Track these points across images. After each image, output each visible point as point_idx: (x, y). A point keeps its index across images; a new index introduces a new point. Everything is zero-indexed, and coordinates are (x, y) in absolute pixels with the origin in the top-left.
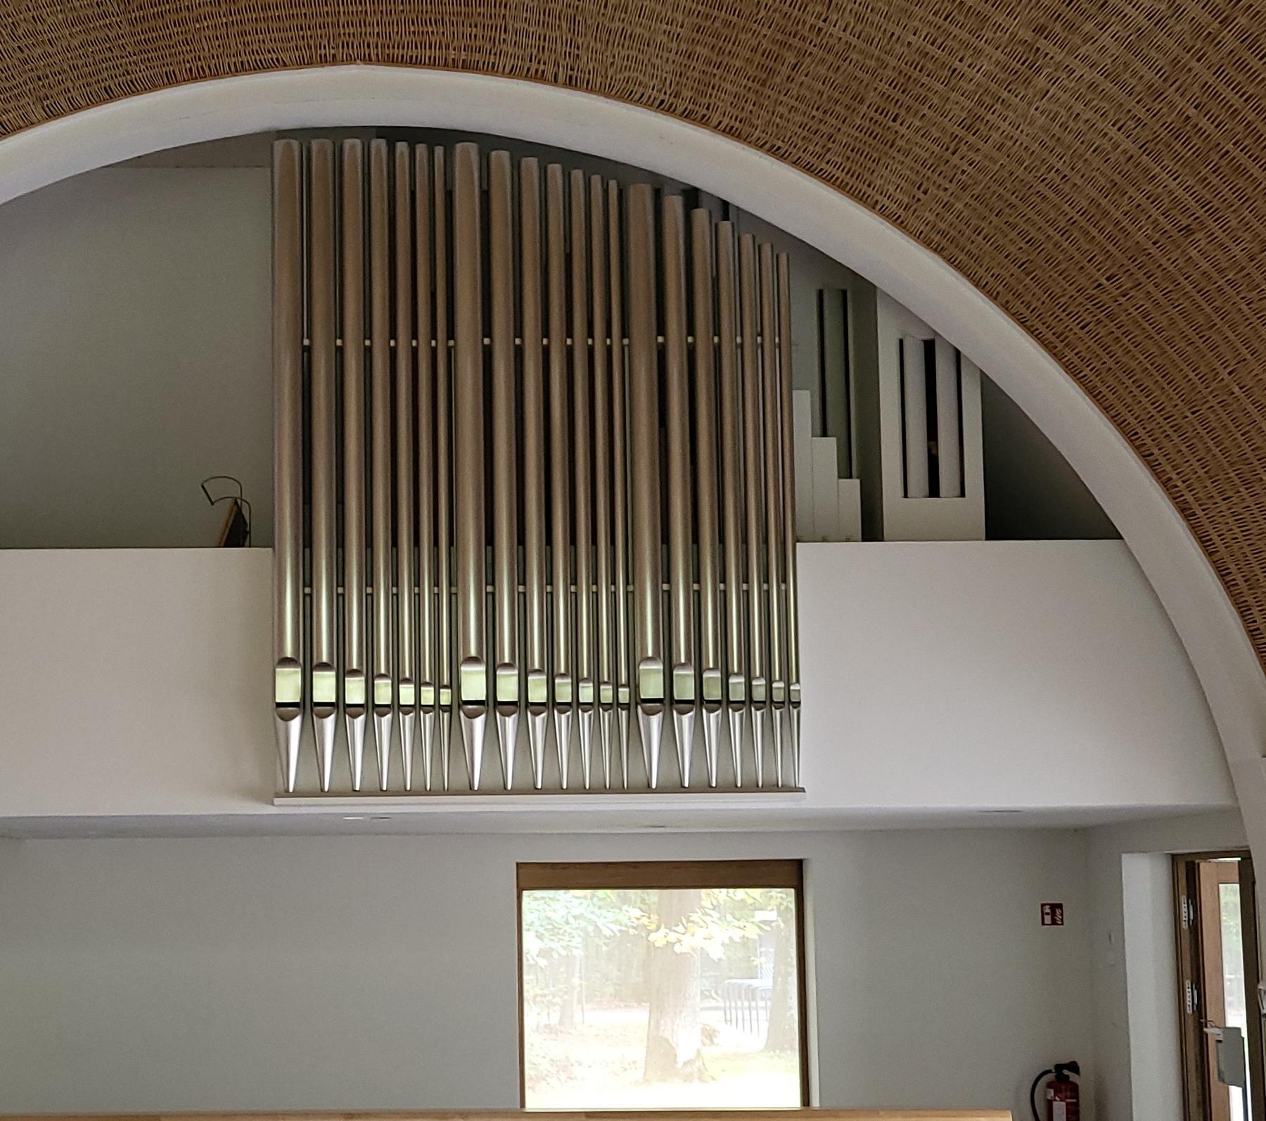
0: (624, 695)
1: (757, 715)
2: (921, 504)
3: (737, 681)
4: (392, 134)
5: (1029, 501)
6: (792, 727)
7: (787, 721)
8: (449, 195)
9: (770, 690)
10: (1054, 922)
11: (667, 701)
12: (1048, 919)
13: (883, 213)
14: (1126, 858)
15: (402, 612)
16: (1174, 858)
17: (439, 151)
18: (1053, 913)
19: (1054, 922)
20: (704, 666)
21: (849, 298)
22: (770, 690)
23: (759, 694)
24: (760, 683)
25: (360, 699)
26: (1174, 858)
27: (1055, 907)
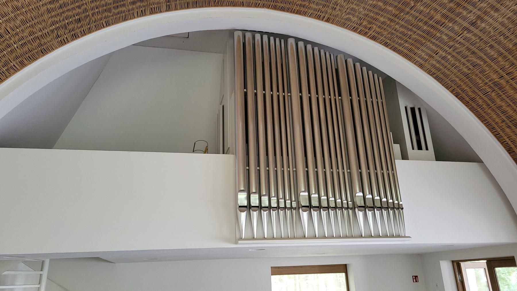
0: (294, 205)
1: (391, 212)
2: (416, 151)
3: (282, 201)
4: (269, 34)
5: (450, 150)
6: (401, 216)
7: (399, 213)
8: (337, 70)
9: (278, 202)
10: (416, 281)
11: (248, 207)
12: (415, 280)
13: (416, 63)
14: (441, 262)
15: (341, 183)
16: (453, 262)
17: (282, 41)
18: (415, 278)
19: (416, 281)
20: (261, 194)
21: (390, 84)
22: (278, 202)
23: (288, 206)
24: (288, 202)
25: (276, 205)
26: (453, 262)
27: (416, 277)
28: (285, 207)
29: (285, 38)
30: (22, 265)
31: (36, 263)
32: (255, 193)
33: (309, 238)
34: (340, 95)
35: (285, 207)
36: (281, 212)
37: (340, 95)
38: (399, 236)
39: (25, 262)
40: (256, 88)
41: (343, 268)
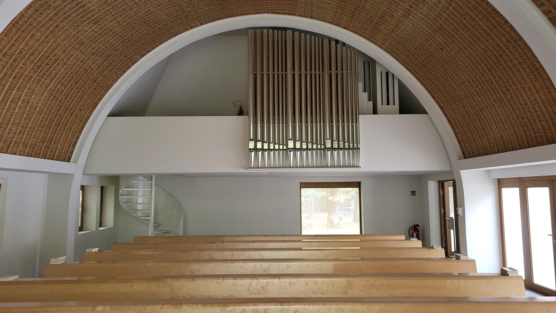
3: (347, 144)
4: (273, 28)
5: (408, 106)
17: (283, 32)
18: (413, 193)
27: (414, 192)
28: (349, 148)
29: (285, 29)
30: (141, 178)
31: (149, 177)
32: (291, 140)
33: (330, 167)
34: (286, 71)
35: (349, 148)
36: (319, 151)
37: (323, 70)
38: (354, 166)
39: (143, 176)
40: (331, 70)
41: (357, 185)
